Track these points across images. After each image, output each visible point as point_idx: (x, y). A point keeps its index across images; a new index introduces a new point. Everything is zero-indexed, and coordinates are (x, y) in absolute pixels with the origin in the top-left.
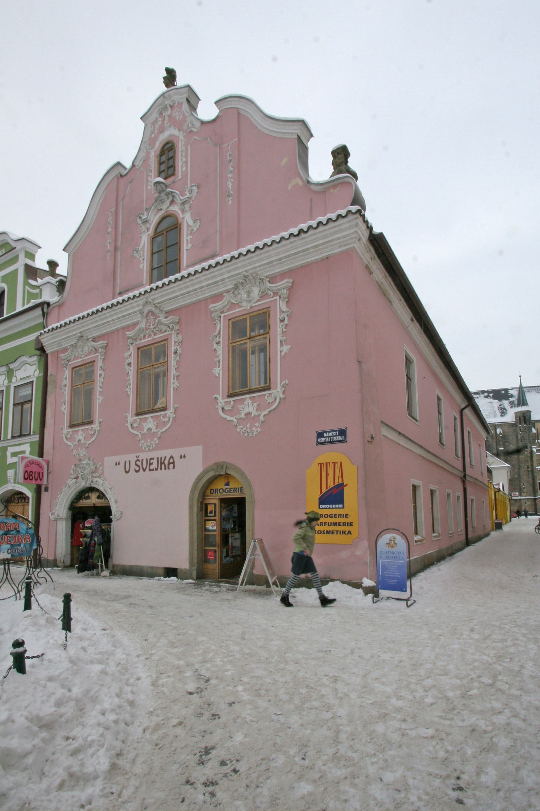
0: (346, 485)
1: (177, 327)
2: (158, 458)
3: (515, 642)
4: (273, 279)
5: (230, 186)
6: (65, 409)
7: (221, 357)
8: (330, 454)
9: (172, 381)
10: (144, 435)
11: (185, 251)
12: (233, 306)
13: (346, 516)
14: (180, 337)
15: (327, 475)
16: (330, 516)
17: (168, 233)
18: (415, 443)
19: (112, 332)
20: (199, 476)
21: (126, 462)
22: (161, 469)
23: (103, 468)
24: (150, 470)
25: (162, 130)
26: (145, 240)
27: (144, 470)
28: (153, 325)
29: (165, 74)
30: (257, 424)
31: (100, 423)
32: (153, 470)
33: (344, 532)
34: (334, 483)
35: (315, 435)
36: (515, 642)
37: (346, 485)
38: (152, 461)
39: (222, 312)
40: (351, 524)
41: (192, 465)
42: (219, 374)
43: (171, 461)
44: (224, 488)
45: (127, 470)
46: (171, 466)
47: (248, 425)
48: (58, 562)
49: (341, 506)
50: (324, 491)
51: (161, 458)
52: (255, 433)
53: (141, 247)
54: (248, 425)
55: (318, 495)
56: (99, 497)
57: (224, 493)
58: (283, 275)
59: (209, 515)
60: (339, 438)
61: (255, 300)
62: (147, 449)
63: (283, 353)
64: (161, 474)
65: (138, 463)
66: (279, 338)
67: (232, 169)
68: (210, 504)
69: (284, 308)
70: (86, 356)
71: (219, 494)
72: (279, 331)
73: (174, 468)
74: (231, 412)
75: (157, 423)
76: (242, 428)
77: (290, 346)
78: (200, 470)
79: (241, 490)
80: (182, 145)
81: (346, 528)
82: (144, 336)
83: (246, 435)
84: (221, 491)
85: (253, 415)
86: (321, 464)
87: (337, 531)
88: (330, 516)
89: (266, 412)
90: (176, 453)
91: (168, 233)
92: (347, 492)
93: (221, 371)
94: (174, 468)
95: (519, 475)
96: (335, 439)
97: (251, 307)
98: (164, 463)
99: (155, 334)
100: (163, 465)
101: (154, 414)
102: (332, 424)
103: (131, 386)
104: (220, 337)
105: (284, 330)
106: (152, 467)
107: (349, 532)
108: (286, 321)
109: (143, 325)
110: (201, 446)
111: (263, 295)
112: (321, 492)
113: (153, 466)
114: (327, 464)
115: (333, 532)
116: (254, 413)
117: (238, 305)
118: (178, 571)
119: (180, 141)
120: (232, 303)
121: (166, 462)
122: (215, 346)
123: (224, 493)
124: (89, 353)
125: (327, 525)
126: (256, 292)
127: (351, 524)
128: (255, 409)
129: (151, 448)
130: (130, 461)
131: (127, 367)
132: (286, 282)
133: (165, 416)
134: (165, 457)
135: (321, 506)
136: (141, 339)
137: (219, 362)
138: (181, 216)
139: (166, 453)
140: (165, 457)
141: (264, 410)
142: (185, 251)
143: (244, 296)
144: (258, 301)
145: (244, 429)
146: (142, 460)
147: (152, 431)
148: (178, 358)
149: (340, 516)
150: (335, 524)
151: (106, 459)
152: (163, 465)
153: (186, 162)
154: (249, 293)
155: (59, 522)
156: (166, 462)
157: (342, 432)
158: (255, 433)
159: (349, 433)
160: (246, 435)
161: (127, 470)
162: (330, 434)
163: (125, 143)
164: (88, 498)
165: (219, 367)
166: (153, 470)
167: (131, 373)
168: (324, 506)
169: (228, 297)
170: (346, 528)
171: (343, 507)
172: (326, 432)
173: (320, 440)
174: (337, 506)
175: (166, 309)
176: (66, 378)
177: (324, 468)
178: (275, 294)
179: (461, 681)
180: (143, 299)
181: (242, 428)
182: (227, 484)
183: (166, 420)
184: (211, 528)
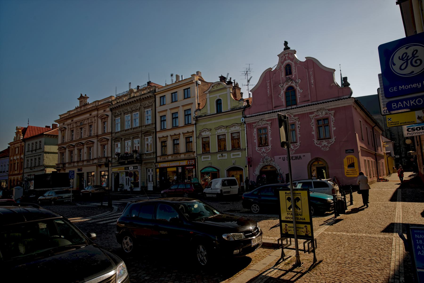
3: (259, 233)
4: (329, 110)
10: (322, 147)
12: (317, 116)
14: (299, 123)
17: (291, 90)
18: (377, 169)
19: (273, 119)
25: (285, 60)
26: (282, 92)
29: (284, 43)
36: (259, 233)
56: (271, 168)
58: (332, 109)
66: (332, 126)
69: (333, 118)
72: (332, 124)
74: (319, 144)
78: (310, 160)
90: (302, 155)
91: (291, 90)
92: (355, 164)
95: (400, 144)
111: (326, 114)
113: (294, 158)
116: (326, 145)
124: (264, 125)
126: (324, 113)
132: (333, 112)
139: (299, 155)
143: (320, 113)
153: (296, 72)
154: (322, 113)
163: (273, 63)
164: (267, 168)
169: (315, 114)
178: (330, 114)
179: (382, 157)
182: (318, 163)
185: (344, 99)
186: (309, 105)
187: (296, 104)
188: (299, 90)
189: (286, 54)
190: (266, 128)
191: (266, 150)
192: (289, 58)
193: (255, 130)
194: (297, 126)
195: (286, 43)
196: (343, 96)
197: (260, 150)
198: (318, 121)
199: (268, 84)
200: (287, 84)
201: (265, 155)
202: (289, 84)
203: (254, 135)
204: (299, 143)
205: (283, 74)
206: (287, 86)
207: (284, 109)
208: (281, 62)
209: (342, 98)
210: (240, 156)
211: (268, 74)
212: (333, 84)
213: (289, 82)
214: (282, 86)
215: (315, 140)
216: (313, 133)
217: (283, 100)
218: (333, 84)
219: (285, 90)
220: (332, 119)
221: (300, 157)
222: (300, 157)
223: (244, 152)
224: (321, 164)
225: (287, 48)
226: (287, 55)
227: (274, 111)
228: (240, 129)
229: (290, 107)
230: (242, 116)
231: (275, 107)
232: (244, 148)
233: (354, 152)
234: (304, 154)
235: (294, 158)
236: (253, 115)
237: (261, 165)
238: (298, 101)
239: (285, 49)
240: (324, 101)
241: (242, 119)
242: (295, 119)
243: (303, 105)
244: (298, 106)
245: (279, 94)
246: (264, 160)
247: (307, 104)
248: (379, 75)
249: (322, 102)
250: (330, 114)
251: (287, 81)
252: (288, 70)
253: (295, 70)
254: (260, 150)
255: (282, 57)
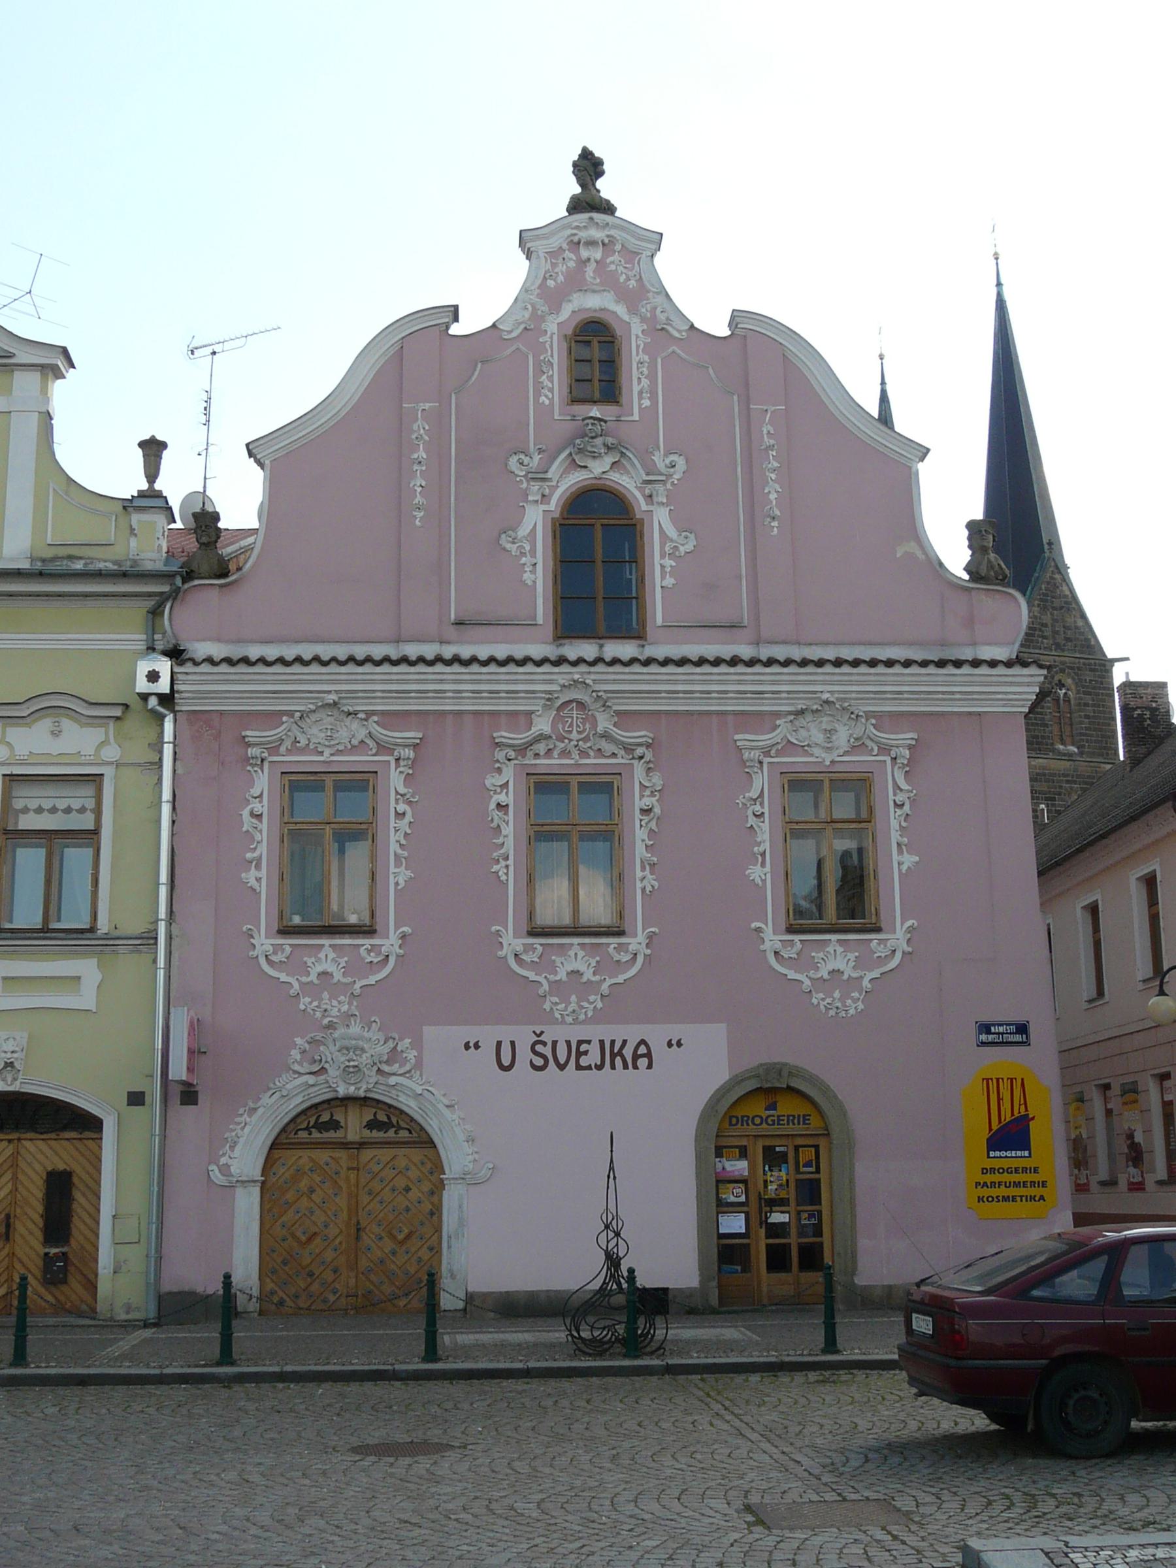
0: (1033, 1118)
1: (649, 756)
2: (602, 1042)
4: (882, 720)
5: (773, 496)
6: (258, 880)
7: (766, 846)
8: (1003, 1061)
9: (639, 874)
10: (556, 986)
11: (658, 590)
12: (789, 747)
13: (1036, 1170)
14: (657, 780)
15: (999, 1099)
16: (1009, 1171)
20: (722, 1087)
21: (499, 1044)
22: (613, 1067)
23: (420, 1052)
24: (579, 1067)
25: (576, 282)
27: (562, 1067)
28: (579, 732)
30: (855, 995)
31: (404, 937)
32: (589, 1068)
33: (1032, 1198)
34: (1012, 1114)
35: (973, 1030)
37: (1033, 1118)
38: (583, 1048)
39: (767, 754)
40: (1044, 1184)
41: (701, 1064)
42: (764, 881)
43: (642, 1050)
44: (764, 1114)
45: (506, 1061)
46: (642, 1063)
47: (837, 994)
48: (241, 1300)
49: (1027, 1153)
50: (995, 1127)
51: (613, 1042)
52: (852, 1011)
53: (523, 531)
54: (837, 994)
55: (986, 1134)
56: (372, 1125)
57: (764, 1125)
58: (896, 720)
59: (802, 1169)
60: (1018, 1038)
61: (841, 752)
62: (569, 1019)
63: (904, 868)
64: (616, 1078)
65: (539, 1048)
66: (895, 836)
67: (776, 464)
68: (725, 1147)
70: (339, 752)
71: (751, 1126)
72: (894, 824)
73: (650, 1066)
75: (598, 962)
76: (823, 999)
77: (917, 859)
79: (804, 1120)
80: (638, 347)
81: (1036, 1192)
82: (549, 752)
83: (832, 1013)
84: (757, 1121)
85: (845, 977)
86: (988, 1080)
87: (1021, 1197)
88: (1009, 1171)
89: (875, 974)
93: (769, 876)
94: (650, 1066)
96: (1011, 1038)
97: (832, 762)
98: (620, 1053)
99: (583, 754)
100: (618, 1060)
101: (587, 940)
102: (1006, 1012)
103: (510, 862)
104: (762, 804)
105: (904, 824)
106: (584, 1061)
107: (1042, 1198)
108: (907, 808)
109: (543, 725)
110: (724, 1025)
111: (858, 746)
112: (991, 1129)
114: (998, 1080)
115: (1014, 1199)
116: (849, 972)
117: (803, 749)
118: (670, 1296)
119: (633, 338)
120: (789, 741)
121: (628, 1052)
122: (752, 821)
123: (764, 1125)
124: (353, 749)
125: (1003, 1187)
126: (842, 737)
127: (1044, 1184)
128: (852, 964)
129: (582, 1017)
130: (513, 1043)
131: (497, 815)
133: (620, 948)
134: (625, 1042)
135: (992, 1154)
136: (537, 755)
137: (763, 854)
138: (644, 507)
139: (631, 1033)
140: (625, 1042)
141: (871, 970)
142: (658, 590)
143: (819, 737)
144: (846, 753)
145: (829, 1000)
146: (555, 1043)
147: (584, 979)
148: (653, 825)
149: (1025, 1170)
150: (1017, 1184)
151: (430, 1032)
152: (618, 1060)
155: (240, 1191)
156: (628, 1052)
157: (1022, 1029)
158: (852, 1011)
159: (1032, 1029)
160: (832, 1013)
161: (506, 1061)
162: (1001, 1029)
165: (763, 865)
166: (589, 1068)
167: (508, 830)
168: (997, 1153)
169: (783, 729)
170: (1036, 1192)
171: (1030, 1156)
172: (994, 1025)
173: (983, 1037)
174: (1019, 1153)
175: (615, 708)
176: (261, 796)
177: (993, 1086)
180: (577, 673)
181: (823, 999)
182: (772, 1106)
183: (625, 958)
184: (732, 1199)
185: (976, 663)
186: (734, 661)
187: (638, 635)
188: (672, 532)
189: (591, 243)
190: (360, 783)
191: (355, 968)
192: (609, 282)
193: (262, 782)
194: (639, 804)
195: (588, 167)
196: (974, 644)
197: (294, 965)
198: (798, 784)
199: (420, 427)
200: (574, 465)
201: (338, 1007)
202: (599, 468)
203: (247, 822)
204: (641, 937)
205: (553, 383)
206: (576, 479)
207: (537, 651)
208: (541, 294)
209: (967, 654)
210: (86, 998)
211: (419, 350)
212: (912, 547)
213: (595, 456)
214: (539, 476)
215: (768, 930)
216: (756, 873)
217: (537, 574)
218: (912, 547)
219: (554, 505)
220: (897, 787)
221: (643, 1054)
222: (643, 1054)
223: (128, 964)
224: (791, 1119)
225: (589, 203)
226: (597, 254)
227: (448, 652)
228: (112, 753)
229: (588, 649)
230: (138, 639)
231: (459, 623)
232: (135, 926)
233: (1026, 1043)
234: (675, 1031)
235: (593, 1057)
236: (254, 652)
237: (292, 1093)
238: (657, 612)
239: (576, 206)
240: (848, 653)
241: (143, 667)
242: (628, 749)
243: (693, 651)
244: (650, 651)
245: (509, 528)
246: (329, 1052)
247: (727, 651)
248: (972, 526)
249: (830, 654)
250: (884, 749)
251: (582, 442)
252: (596, 359)
253: (652, 377)
254: (294, 965)
255: (554, 254)
